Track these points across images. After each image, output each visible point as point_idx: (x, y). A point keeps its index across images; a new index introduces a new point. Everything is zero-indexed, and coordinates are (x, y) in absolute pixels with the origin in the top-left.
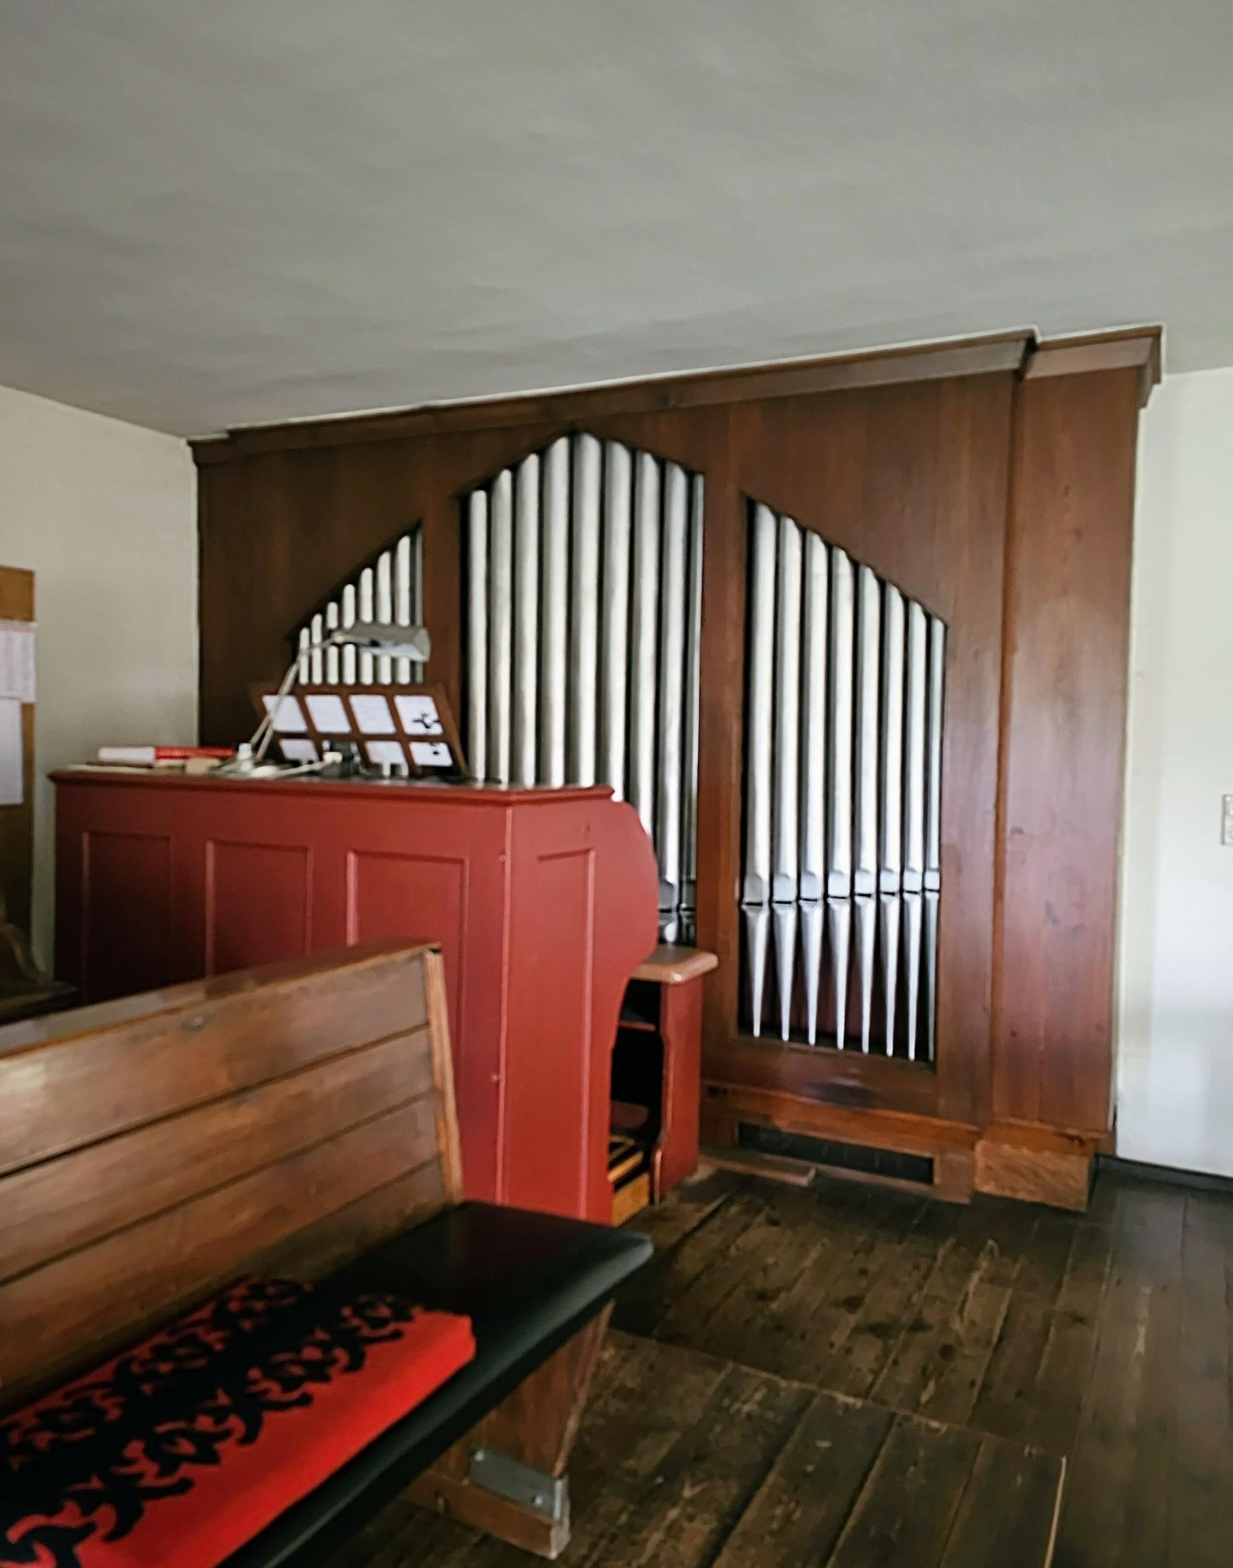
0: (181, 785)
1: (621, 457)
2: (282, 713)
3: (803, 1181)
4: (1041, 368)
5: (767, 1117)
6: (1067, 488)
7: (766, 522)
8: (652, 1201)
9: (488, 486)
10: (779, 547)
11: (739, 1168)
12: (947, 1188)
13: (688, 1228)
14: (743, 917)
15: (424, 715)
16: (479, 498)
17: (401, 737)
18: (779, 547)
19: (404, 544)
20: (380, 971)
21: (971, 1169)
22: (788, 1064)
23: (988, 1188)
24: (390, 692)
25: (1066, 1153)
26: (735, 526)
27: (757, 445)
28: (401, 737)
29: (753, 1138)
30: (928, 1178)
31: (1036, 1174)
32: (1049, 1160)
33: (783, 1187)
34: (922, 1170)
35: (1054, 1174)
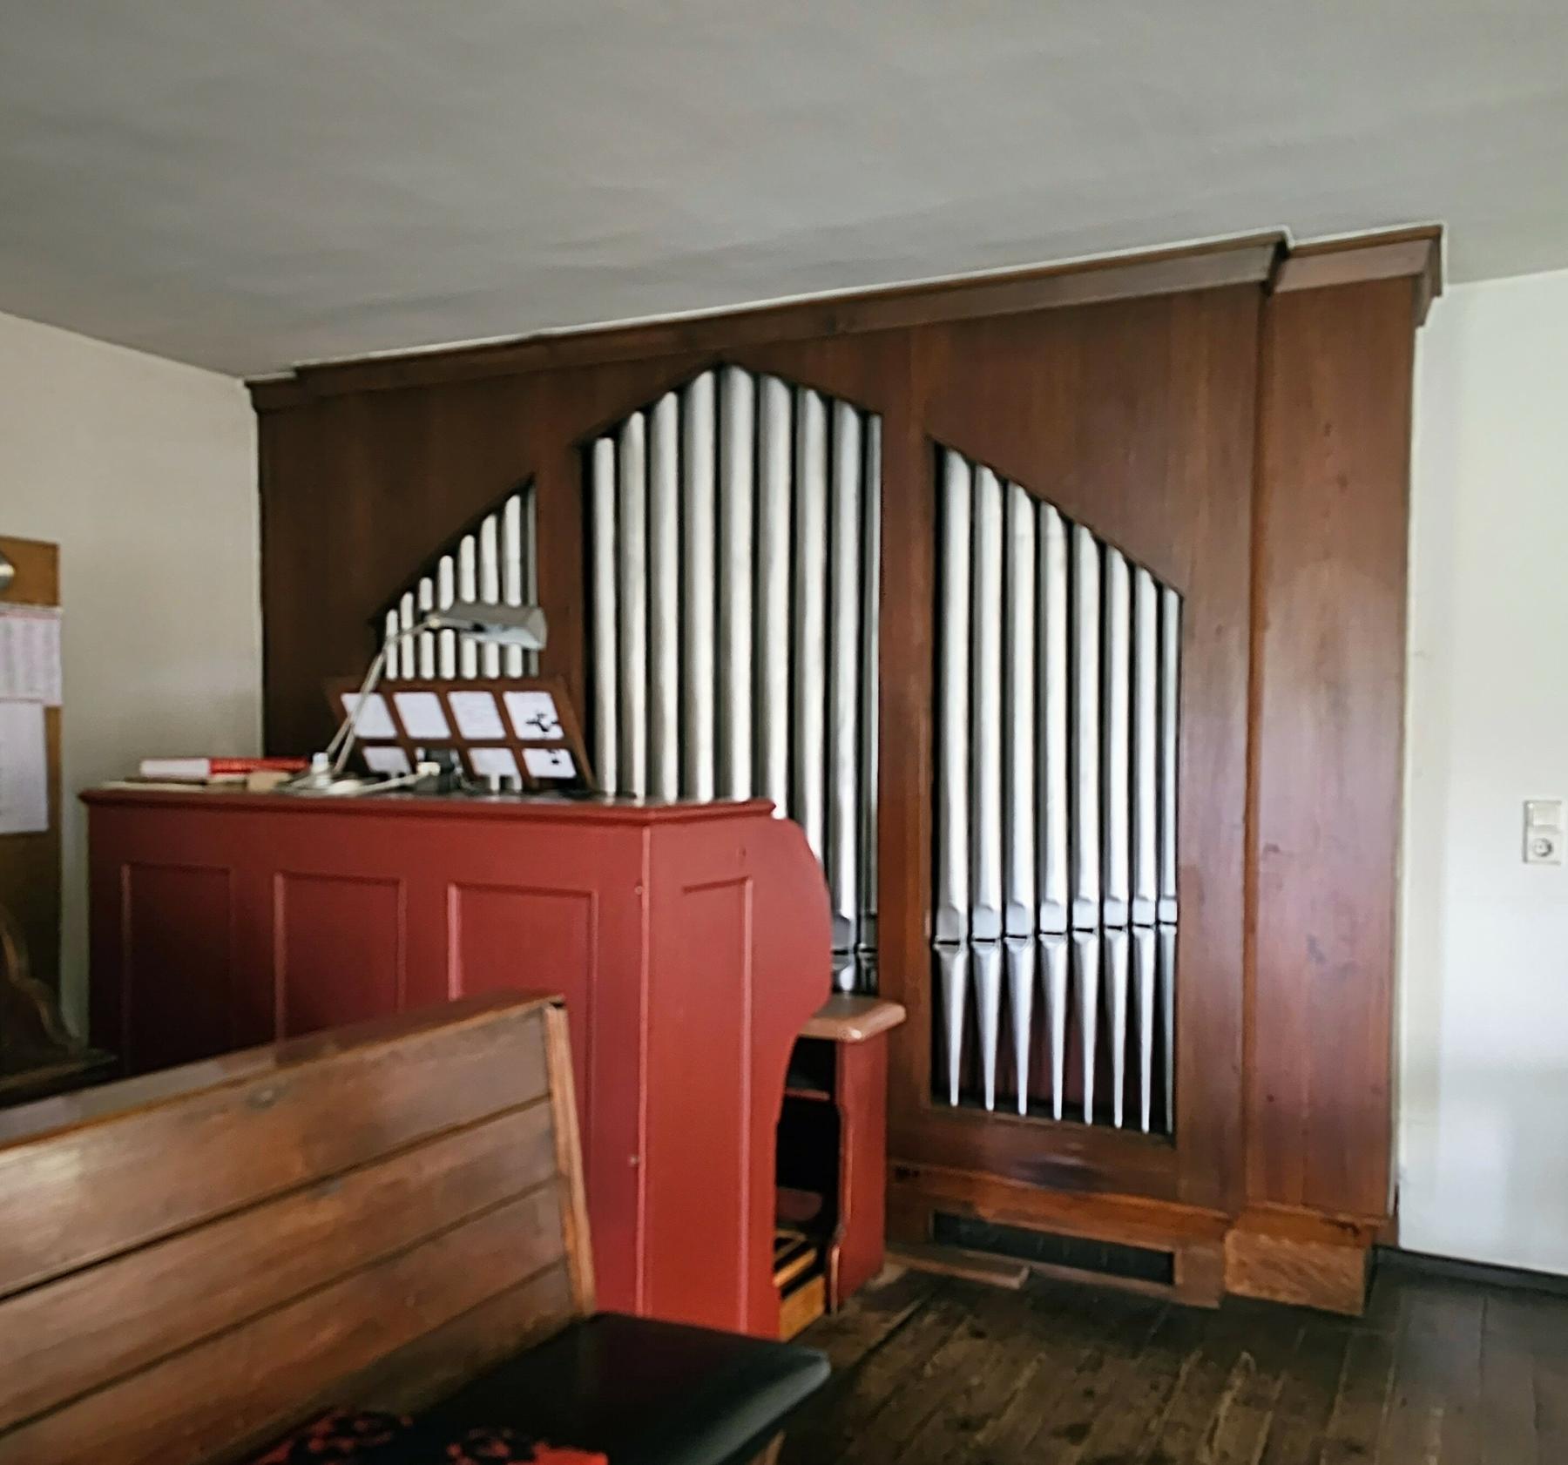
0: (242, 805)
1: (778, 395)
2: (365, 714)
3: (1014, 1283)
4: (1294, 278)
5: (968, 1205)
6: (1328, 427)
7: (958, 472)
8: (828, 1310)
9: (616, 433)
10: (976, 505)
11: (934, 1267)
12: (1192, 1289)
13: (873, 1342)
14: (936, 959)
15: (541, 716)
16: (604, 449)
17: (513, 743)
18: (976, 505)
19: (513, 505)
20: (490, 1031)
21: (1220, 1265)
22: (994, 1140)
23: (1242, 1289)
24: (498, 687)
25: (1336, 1243)
26: (919, 478)
27: (949, 377)
28: (513, 743)
29: (951, 1231)
30: (1167, 1277)
31: (1300, 1271)
32: (1316, 1253)
33: (989, 1290)
34: (1162, 1267)
35: (1323, 1270)
